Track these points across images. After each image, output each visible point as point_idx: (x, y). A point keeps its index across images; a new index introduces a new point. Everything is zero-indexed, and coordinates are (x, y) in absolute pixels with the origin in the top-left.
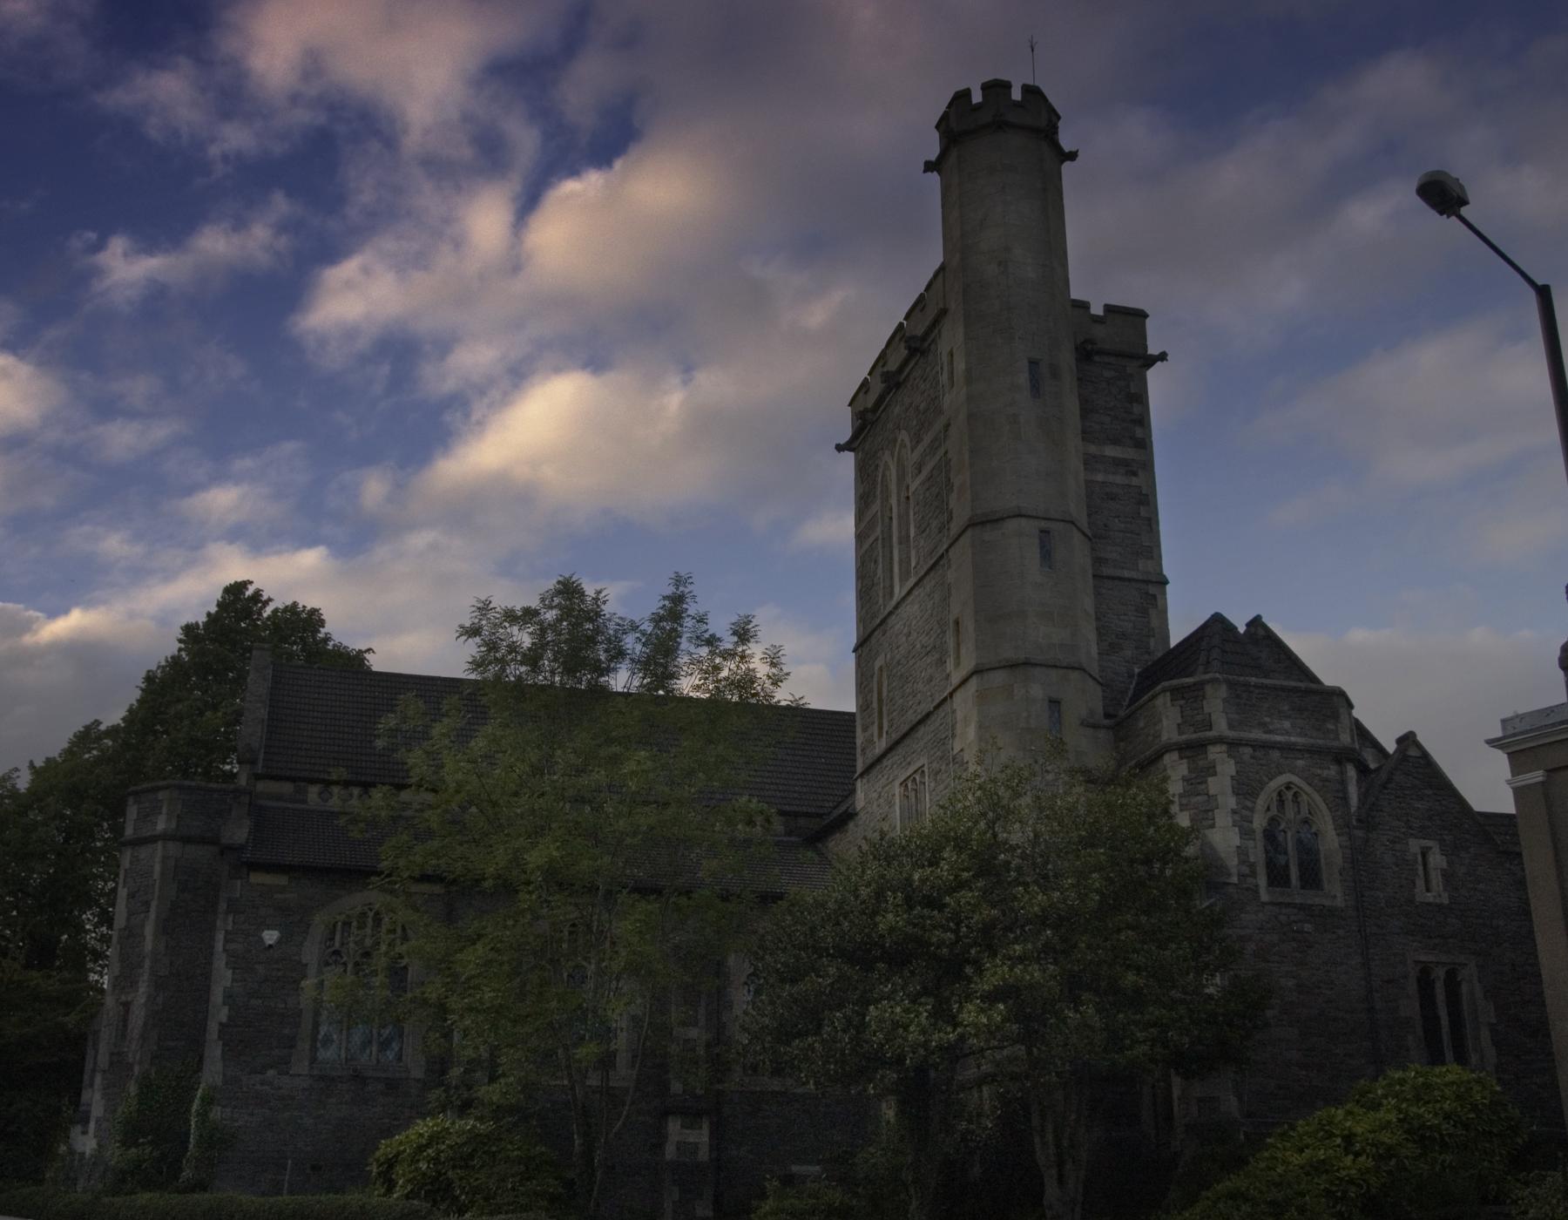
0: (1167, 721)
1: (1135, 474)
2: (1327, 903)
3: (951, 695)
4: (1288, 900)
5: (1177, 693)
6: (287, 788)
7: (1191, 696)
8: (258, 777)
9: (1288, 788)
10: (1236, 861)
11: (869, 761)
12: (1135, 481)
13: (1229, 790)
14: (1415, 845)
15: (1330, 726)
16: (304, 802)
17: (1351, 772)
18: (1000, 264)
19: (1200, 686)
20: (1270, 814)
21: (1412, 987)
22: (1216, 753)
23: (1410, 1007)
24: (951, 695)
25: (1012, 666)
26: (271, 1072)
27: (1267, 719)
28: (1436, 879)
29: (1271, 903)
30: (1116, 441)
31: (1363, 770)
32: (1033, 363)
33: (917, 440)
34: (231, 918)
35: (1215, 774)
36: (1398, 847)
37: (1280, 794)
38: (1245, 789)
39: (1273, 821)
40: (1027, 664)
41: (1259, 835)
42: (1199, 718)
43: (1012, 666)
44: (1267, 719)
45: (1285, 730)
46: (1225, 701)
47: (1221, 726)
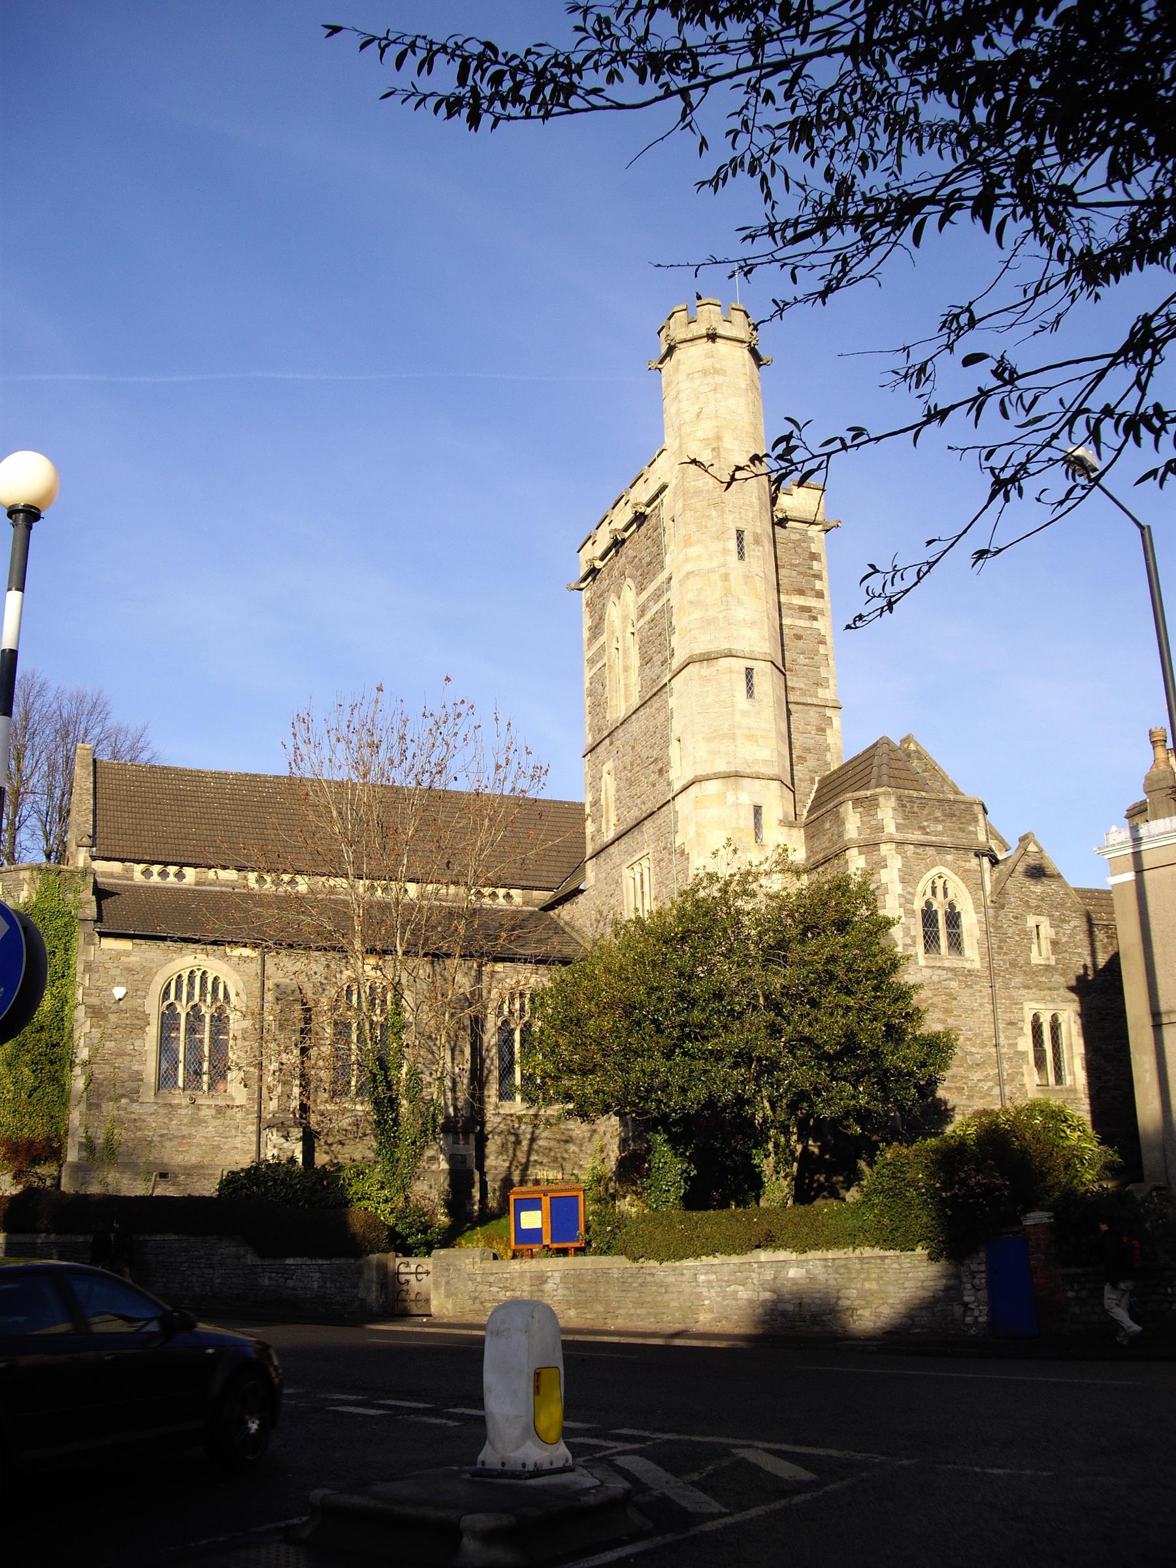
0: (853, 823)
1: (815, 619)
2: (968, 965)
3: (673, 798)
4: (939, 964)
5: (857, 802)
6: (116, 867)
7: (868, 805)
8: (94, 858)
9: (940, 877)
10: (901, 935)
11: (598, 848)
12: (815, 624)
13: (897, 879)
14: (1031, 921)
15: (971, 828)
16: (131, 879)
17: (985, 860)
18: (713, 449)
19: (874, 798)
20: (926, 897)
21: (1028, 1029)
22: (886, 849)
23: (1026, 1043)
24: (673, 798)
25: (726, 776)
26: (123, 1101)
27: (925, 824)
28: (1046, 946)
29: (927, 967)
30: (801, 592)
31: (994, 862)
32: (740, 534)
33: (641, 589)
34: (87, 976)
35: (885, 866)
36: (1019, 922)
37: (933, 882)
38: (908, 877)
39: (928, 904)
40: (738, 775)
41: (919, 915)
42: (873, 822)
43: (726, 776)
44: (925, 824)
45: (938, 831)
46: (894, 809)
47: (890, 828)
